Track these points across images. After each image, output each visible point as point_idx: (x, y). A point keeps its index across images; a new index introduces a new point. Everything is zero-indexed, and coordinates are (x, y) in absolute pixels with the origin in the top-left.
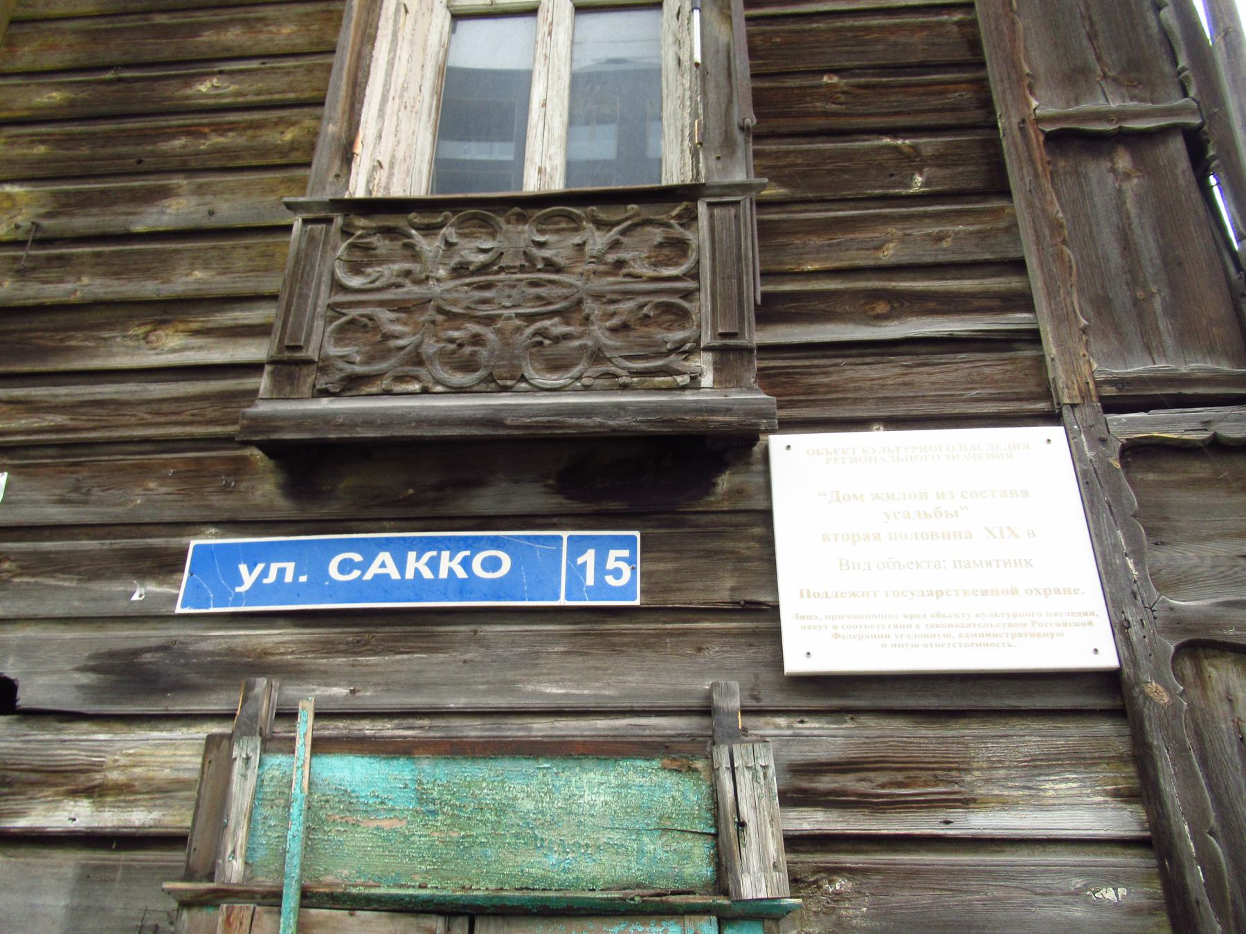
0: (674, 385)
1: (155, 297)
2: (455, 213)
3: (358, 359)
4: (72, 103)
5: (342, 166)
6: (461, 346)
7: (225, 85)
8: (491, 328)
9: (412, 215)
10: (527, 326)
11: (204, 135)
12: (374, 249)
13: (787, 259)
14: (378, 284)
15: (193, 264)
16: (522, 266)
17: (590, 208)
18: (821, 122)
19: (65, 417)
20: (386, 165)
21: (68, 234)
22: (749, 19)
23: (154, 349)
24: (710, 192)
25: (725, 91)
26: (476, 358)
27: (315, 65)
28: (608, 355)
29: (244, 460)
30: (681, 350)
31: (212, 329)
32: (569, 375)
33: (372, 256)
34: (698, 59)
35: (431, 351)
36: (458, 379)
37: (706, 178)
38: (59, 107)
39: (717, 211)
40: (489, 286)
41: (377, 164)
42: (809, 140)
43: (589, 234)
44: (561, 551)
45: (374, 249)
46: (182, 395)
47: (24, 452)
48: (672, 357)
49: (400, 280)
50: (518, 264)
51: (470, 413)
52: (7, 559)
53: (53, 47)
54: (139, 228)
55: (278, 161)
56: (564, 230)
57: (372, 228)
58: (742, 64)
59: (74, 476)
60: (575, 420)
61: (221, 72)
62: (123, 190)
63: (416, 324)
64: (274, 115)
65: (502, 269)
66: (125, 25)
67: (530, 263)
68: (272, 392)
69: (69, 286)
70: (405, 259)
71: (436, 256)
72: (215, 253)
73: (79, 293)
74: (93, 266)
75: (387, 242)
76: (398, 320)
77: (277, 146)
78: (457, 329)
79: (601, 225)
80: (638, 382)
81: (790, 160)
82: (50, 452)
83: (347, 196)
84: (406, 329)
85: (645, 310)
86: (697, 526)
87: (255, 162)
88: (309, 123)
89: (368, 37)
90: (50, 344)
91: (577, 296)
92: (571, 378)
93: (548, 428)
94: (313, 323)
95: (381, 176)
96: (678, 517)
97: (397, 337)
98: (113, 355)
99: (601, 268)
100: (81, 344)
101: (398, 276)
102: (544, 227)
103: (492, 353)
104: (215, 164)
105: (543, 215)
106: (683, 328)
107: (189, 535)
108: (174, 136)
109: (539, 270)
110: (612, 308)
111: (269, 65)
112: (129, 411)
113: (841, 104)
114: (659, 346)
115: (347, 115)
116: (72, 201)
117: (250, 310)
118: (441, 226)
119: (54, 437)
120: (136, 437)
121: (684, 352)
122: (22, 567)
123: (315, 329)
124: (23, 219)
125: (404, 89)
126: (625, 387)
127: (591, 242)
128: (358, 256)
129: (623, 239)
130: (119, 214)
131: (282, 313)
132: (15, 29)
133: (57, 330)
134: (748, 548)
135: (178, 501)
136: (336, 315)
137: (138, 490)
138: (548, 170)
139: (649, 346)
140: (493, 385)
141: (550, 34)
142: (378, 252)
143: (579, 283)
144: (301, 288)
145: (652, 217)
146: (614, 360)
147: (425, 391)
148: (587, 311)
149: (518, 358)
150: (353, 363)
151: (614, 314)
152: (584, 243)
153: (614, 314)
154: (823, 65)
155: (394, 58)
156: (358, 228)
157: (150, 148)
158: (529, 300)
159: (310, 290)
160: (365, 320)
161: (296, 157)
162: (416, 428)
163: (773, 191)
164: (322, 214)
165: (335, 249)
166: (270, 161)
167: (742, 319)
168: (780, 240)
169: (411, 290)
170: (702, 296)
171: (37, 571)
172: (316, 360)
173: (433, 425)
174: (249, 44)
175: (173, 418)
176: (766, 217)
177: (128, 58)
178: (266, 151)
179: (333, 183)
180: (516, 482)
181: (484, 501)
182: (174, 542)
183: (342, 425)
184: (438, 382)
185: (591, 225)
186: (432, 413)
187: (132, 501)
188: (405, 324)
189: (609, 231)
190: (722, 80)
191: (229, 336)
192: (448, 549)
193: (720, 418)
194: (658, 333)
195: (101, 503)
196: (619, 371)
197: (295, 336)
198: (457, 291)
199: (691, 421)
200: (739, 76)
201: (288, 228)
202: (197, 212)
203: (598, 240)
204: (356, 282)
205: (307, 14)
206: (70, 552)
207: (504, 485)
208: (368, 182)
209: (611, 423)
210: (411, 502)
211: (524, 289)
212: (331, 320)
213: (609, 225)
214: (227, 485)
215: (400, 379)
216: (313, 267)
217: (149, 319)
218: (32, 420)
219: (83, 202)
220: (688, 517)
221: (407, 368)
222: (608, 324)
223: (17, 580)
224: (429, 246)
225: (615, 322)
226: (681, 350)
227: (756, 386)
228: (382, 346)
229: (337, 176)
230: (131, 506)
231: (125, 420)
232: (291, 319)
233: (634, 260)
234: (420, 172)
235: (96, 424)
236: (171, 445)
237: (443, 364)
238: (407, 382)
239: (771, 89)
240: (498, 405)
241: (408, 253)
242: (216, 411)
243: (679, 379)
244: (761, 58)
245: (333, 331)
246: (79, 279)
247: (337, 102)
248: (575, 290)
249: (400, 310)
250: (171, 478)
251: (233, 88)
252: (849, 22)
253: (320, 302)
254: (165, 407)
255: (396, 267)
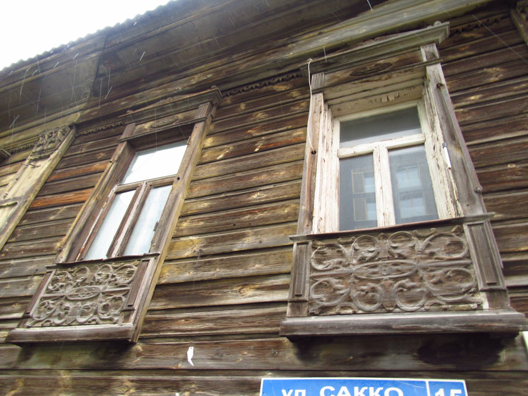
0: (470, 309)
1: (242, 275)
2: (356, 237)
3: (325, 299)
4: (211, 206)
5: (309, 221)
6: (367, 293)
7: (262, 195)
8: (379, 284)
9: (339, 239)
10: (395, 283)
11: (256, 214)
12: (326, 253)
13: (510, 246)
14: (329, 268)
15: (255, 262)
16: (388, 257)
17: (414, 231)
18: (512, 184)
19: (213, 324)
20: (323, 219)
21: (212, 253)
22: (468, 146)
23: (243, 296)
24: (468, 220)
25: (464, 177)
26: (374, 298)
27: (294, 184)
28: (435, 295)
29: (279, 342)
30: (469, 292)
31: (264, 287)
32: (418, 305)
33: (325, 256)
34: (449, 166)
35: (355, 295)
36: (368, 307)
37: (464, 214)
38: (207, 208)
39: (473, 228)
40: (375, 266)
41: (320, 219)
42: (508, 192)
43: (415, 242)
44: (426, 389)
45: (326, 253)
46: (254, 314)
47: (198, 338)
48: (466, 295)
49: (338, 266)
50: (386, 256)
51: (375, 323)
52: (193, 383)
53: (204, 188)
54: (235, 249)
55: (283, 221)
56: (404, 241)
57: (324, 245)
58: (470, 165)
59: (217, 348)
60: (424, 326)
61: (260, 191)
62: (229, 236)
63: (347, 284)
64: (280, 204)
65: (379, 259)
66: (227, 178)
67: (392, 256)
68: (291, 314)
69: (212, 273)
70: (339, 257)
71: (351, 255)
72: (263, 257)
73: (216, 275)
74: (220, 265)
75: (330, 250)
76: (339, 283)
77: (282, 215)
78: (365, 285)
79: (420, 238)
80: (451, 307)
81: (500, 202)
82: (208, 338)
83: (312, 234)
84: (343, 286)
85: (448, 274)
86: (494, 378)
87: (275, 222)
88: (293, 206)
89: (313, 173)
90: (207, 295)
91: (415, 269)
92: (419, 306)
93: (413, 329)
94: (305, 285)
95: (322, 222)
96: (483, 373)
97: (340, 290)
98: (228, 299)
99: (424, 256)
100: (217, 294)
101: (337, 264)
102: (395, 240)
103: (381, 295)
104: (261, 224)
105: (394, 235)
106: (468, 281)
107: (261, 375)
108: (246, 215)
109: (396, 259)
110: (432, 273)
111: (277, 186)
112: (235, 321)
113: (520, 175)
114: (458, 290)
115: (308, 202)
116: (212, 241)
117: (277, 279)
118: (352, 242)
119: (209, 332)
120: (238, 332)
121: (471, 293)
122: (199, 387)
123: (306, 287)
124: (197, 248)
125: (326, 189)
126: (445, 310)
127: (417, 245)
128: (319, 256)
129: (431, 243)
130: (229, 245)
131: (292, 280)
132: (192, 184)
133: (208, 289)
134: (525, 391)
135: (256, 360)
136: (314, 281)
137: (240, 355)
138: (387, 214)
139: (453, 290)
140: (384, 310)
141: (379, 161)
142: (327, 254)
143: (415, 263)
144: (299, 271)
145: (443, 233)
146: (438, 297)
147: (355, 313)
148: (421, 275)
149: (393, 297)
150: (323, 301)
151: (434, 276)
152: (414, 246)
153: (434, 276)
154: (506, 161)
155: (322, 179)
156: (318, 245)
157: (238, 220)
158: (394, 272)
159: (302, 271)
160: (326, 283)
161: (290, 218)
162: (353, 329)
163: (497, 216)
164: (304, 241)
165: (310, 254)
166: (281, 221)
167: (496, 276)
168: (505, 237)
169: (342, 270)
170: (474, 266)
171: (205, 389)
172: (308, 300)
173: (360, 328)
174: (269, 179)
175: (252, 324)
176: (495, 227)
177: (229, 189)
178: (278, 217)
179: (306, 228)
180: (398, 354)
181: (385, 363)
182: (255, 378)
183: (321, 329)
184: (360, 309)
185: (416, 238)
186: (359, 323)
187: (239, 360)
188: (342, 284)
189: (424, 240)
190: (462, 172)
191: (270, 290)
192: (372, 386)
193: (497, 324)
194: (457, 284)
195: (227, 360)
196: (441, 302)
197: (299, 291)
198: (362, 269)
199: (482, 326)
200: (470, 171)
201: (292, 246)
202: (255, 242)
203: (420, 245)
204: (320, 267)
205: (289, 167)
206: (216, 381)
207: (393, 355)
208: (318, 226)
209: (442, 327)
210: (352, 363)
211: (391, 267)
212: (312, 284)
213: (424, 238)
214: (274, 353)
215: (343, 308)
216: (303, 262)
217: (240, 284)
218: (201, 325)
219: (216, 241)
220: (488, 373)
221: (346, 303)
222: (432, 281)
223: (197, 392)
224: (348, 251)
225: (434, 280)
226: (469, 292)
227: (511, 308)
228: (334, 294)
229: (308, 225)
230: (238, 362)
231: (234, 325)
232: (296, 283)
233: (438, 252)
234: (335, 219)
235: (224, 327)
236: (251, 336)
237: (361, 301)
238: (346, 309)
239: (484, 173)
240: (387, 319)
241: (339, 254)
242: (267, 321)
243: (472, 305)
244: (476, 161)
245: (313, 288)
246: (216, 270)
247: (304, 198)
248: (414, 266)
249: (339, 278)
250: (252, 350)
251: (265, 196)
252: (514, 142)
253: (307, 276)
254: (249, 320)
255: (336, 260)
